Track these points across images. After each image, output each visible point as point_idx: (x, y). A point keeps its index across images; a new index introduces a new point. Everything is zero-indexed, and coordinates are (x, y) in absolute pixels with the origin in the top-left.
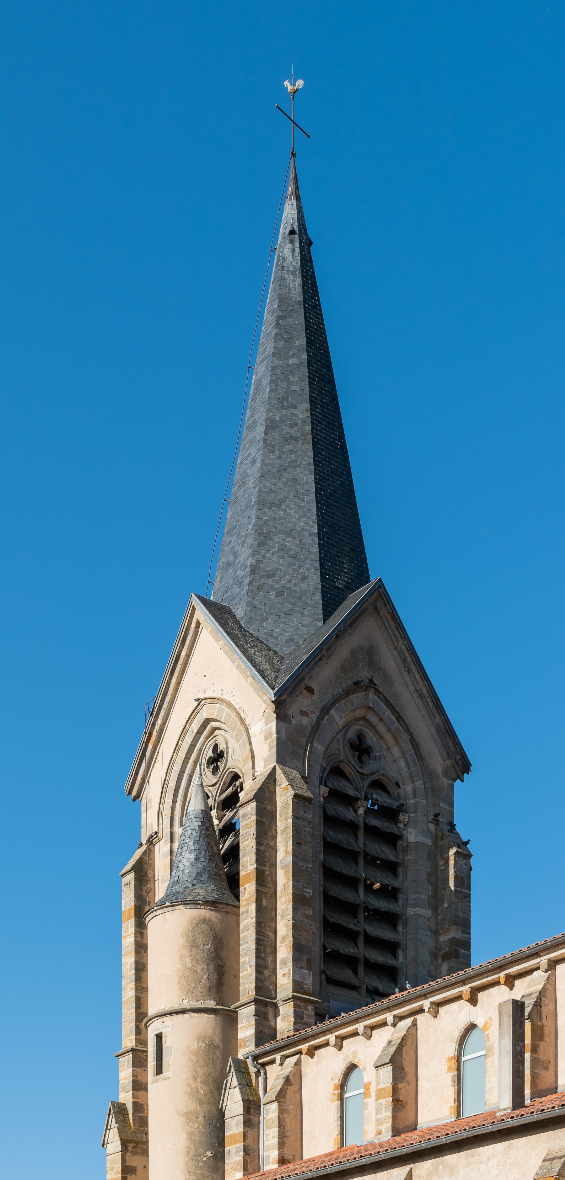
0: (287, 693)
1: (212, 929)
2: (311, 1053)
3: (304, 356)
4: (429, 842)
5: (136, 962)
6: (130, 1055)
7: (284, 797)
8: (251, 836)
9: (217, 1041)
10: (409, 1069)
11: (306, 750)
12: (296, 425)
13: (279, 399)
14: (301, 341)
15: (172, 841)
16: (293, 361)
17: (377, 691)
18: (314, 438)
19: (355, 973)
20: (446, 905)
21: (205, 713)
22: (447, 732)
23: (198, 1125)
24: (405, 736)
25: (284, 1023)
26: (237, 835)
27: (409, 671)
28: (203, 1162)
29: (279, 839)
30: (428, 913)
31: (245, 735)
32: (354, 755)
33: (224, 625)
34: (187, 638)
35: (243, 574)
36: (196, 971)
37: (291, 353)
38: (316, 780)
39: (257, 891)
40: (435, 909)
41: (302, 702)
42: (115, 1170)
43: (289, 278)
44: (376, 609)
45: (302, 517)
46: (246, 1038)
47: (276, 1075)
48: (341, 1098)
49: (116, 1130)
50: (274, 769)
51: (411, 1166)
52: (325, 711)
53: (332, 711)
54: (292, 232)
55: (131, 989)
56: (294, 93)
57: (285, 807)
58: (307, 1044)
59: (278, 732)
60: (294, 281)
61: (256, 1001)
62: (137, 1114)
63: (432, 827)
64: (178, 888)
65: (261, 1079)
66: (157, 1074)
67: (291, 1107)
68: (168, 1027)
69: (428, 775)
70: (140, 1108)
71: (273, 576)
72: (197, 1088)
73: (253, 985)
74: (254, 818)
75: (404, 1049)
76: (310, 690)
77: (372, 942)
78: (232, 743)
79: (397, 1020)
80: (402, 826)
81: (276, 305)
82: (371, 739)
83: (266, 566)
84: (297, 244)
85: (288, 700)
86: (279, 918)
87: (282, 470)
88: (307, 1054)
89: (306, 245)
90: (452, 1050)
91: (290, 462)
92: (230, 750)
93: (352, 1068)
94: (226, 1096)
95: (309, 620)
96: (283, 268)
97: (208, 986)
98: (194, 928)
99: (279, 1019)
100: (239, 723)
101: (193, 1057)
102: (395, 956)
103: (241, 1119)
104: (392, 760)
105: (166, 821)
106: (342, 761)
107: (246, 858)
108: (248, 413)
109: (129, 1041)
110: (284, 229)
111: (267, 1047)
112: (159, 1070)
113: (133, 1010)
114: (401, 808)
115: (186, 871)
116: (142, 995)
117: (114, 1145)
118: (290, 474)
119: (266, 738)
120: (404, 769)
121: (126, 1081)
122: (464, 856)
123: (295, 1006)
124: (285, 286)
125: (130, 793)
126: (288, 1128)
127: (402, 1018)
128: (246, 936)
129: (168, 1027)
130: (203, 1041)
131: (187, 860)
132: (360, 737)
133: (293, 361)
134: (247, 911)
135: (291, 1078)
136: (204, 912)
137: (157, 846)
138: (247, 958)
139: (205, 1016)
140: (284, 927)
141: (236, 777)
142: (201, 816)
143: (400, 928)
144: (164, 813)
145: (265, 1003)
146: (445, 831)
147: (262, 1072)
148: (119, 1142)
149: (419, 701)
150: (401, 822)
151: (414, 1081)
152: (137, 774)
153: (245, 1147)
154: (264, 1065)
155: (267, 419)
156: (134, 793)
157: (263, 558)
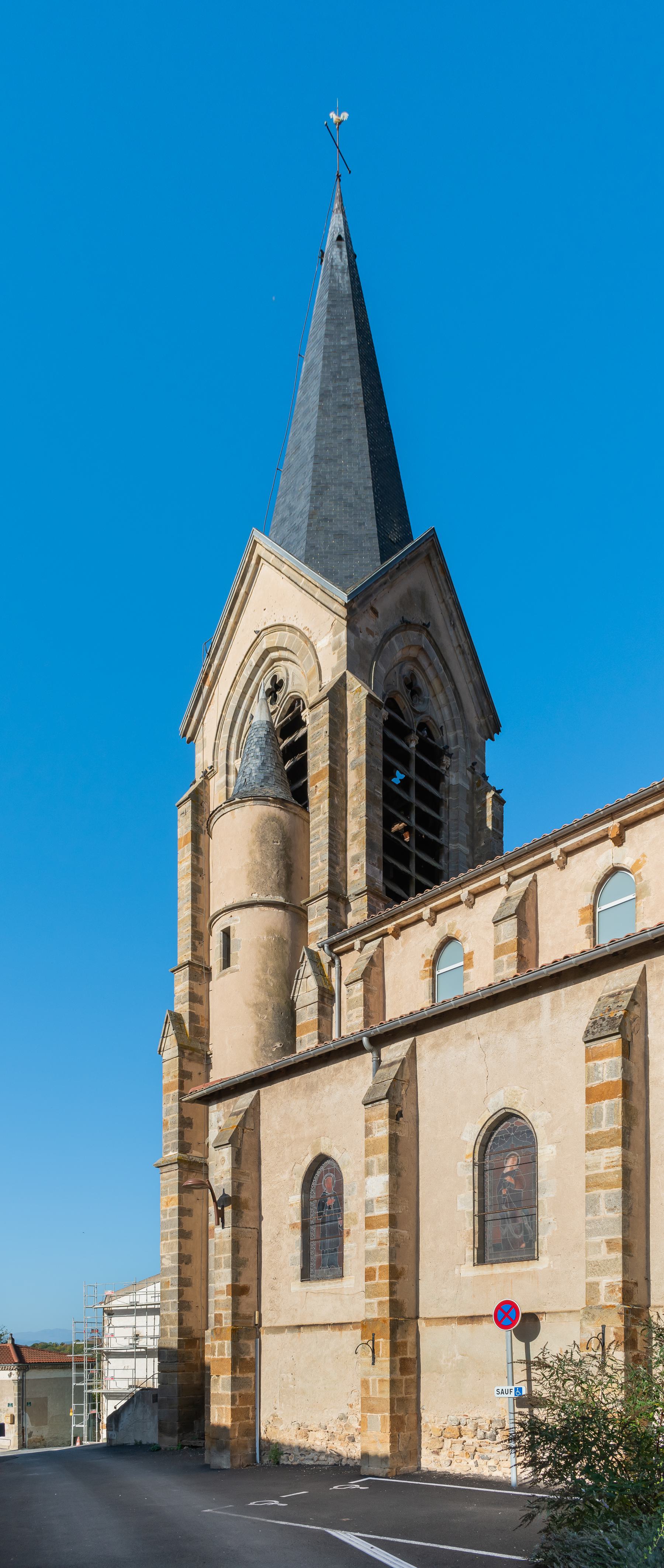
0: (359, 601)
1: (282, 827)
2: (396, 934)
5: (193, 883)
6: (187, 969)
7: (357, 695)
8: (324, 734)
9: (286, 936)
10: (531, 926)
11: (372, 667)
12: (349, 395)
13: (332, 373)
14: (352, 327)
15: (228, 772)
17: (429, 634)
18: (365, 408)
20: (483, 844)
22: (483, 691)
23: (268, 1017)
24: (449, 686)
25: (357, 913)
27: (454, 626)
28: (272, 1052)
29: (350, 741)
30: (466, 850)
31: (310, 653)
32: (407, 692)
36: (266, 866)
37: (342, 336)
39: (330, 787)
40: (472, 848)
42: (171, 1075)
43: (338, 275)
44: (428, 558)
46: (317, 931)
48: (433, 975)
49: (174, 1036)
50: (345, 674)
51: (644, 962)
52: (387, 636)
53: (393, 639)
54: (339, 238)
55: (188, 908)
56: (340, 123)
57: (358, 708)
58: (394, 923)
59: (348, 640)
60: (343, 278)
62: (193, 1024)
63: (470, 774)
65: (334, 971)
66: (224, 968)
67: (375, 988)
68: (236, 920)
69: (467, 727)
71: (331, 521)
72: (266, 980)
73: (327, 878)
74: (327, 716)
75: (527, 902)
76: (376, 613)
79: (511, 879)
80: (444, 768)
81: (326, 297)
82: (421, 683)
84: (344, 249)
85: (358, 610)
86: (349, 817)
87: (337, 431)
88: (392, 934)
90: (586, 899)
91: (345, 425)
92: (290, 677)
94: (298, 986)
96: (332, 266)
97: (277, 881)
98: (263, 824)
99: (350, 915)
100: (303, 643)
101: (262, 949)
103: (315, 1007)
104: (438, 708)
105: (222, 755)
106: (398, 693)
107: (317, 758)
108: (299, 393)
109: (184, 954)
110: (331, 237)
112: (226, 962)
113: (190, 928)
115: (254, 775)
116: (197, 915)
117: (171, 1050)
119: (334, 649)
120: (447, 718)
121: (182, 994)
122: (499, 801)
123: (369, 900)
124: (335, 281)
125: (184, 735)
126: (372, 1008)
127: (514, 877)
128: (318, 832)
129: (238, 922)
130: (273, 935)
132: (413, 675)
134: (319, 808)
135: (375, 959)
136: (273, 810)
137: (212, 781)
138: (318, 853)
139: (274, 911)
140: (356, 827)
142: (266, 726)
143: (443, 861)
144: (220, 743)
145: (337, 896)
146: (479, 781)
147: (337, 961)
148: (177, 1047)
149: (460, 657)
150: (444, 765)
151: (535, 939)
152: (192, 716)
153: (319, 1034)
154: (339, 954)
155: (321, 388)
156: (189, 735)
157: (321, 504)
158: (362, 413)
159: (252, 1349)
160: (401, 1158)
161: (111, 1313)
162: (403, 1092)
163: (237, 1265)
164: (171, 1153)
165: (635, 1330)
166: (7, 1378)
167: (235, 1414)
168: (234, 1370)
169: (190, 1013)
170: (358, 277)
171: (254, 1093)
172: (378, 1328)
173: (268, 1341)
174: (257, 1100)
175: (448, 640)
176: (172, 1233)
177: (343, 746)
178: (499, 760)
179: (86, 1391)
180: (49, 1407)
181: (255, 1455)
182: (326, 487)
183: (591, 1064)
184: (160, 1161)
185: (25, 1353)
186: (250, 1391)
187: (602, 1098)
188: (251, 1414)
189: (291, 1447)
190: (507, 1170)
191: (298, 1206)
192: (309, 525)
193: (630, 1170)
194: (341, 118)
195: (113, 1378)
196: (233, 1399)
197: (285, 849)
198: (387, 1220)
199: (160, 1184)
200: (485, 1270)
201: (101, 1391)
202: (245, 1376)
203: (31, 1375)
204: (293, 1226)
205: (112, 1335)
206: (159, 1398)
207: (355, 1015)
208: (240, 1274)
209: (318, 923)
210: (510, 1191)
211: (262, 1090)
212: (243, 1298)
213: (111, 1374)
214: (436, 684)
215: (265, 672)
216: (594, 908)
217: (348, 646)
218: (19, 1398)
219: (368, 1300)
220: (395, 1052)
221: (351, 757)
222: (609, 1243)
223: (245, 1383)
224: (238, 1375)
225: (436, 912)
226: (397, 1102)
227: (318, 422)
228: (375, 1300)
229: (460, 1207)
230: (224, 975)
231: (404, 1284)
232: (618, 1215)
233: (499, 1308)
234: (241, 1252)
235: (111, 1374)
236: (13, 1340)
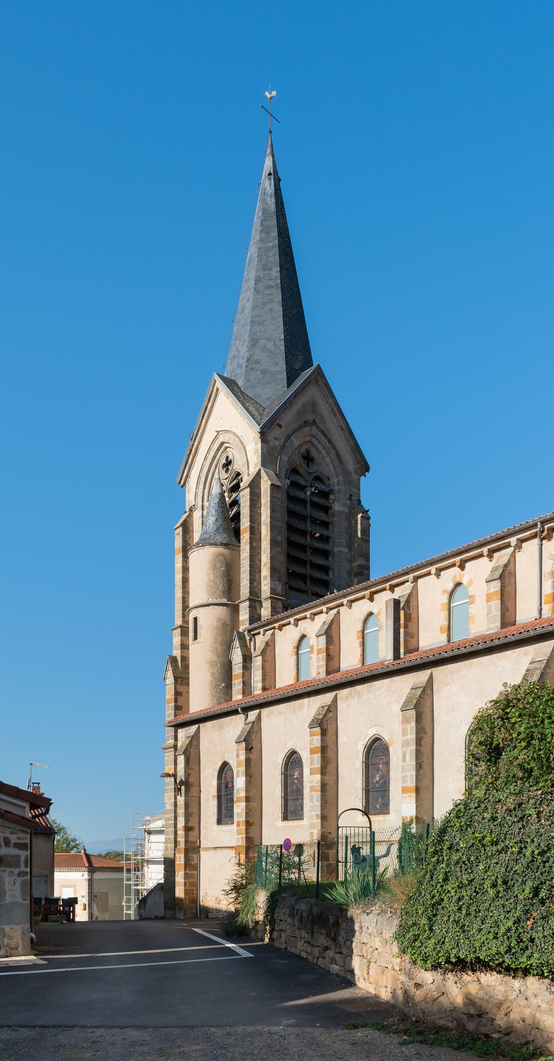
1: (225, 559)
2: (280, 628)
3: (277, 242)
4: (347, 510)
5: (183, 577)
9: (228, 622)
10: (335, 637)
12: (272, 279)
14: (275, 233)
15: (203, 509)
16: (270, 245)
17: (317, 426)
19: (305, 583)
21: (221, 439)
22: (356, 449)
23: (217, 668)
24: (333, 452)
25: (265, 612)
26: (239, 507)
27: (335, 415)
29: (262, 509)
30: (346, 550)
32: (304, 462)
33: (232, 390)
34: (212, 397)
35: (243, 362)
38: (283, 476)
39: (250, 538)
41: (275, 432)
43: (268, 199)
44: (316, 381)
45: (276, 330)
47: (260, 640)
50: (260, 470)
52: (288, 437)
53: (292, 438)
54: (270, 174)
56: (271, 98)
57: (266, 491)
59: (262, 449)
60: (271, 201)
61: (250, 599)
63: (348, 502)
64: (205, 536)
65: (252, 643)
67: (269, 659)
69: (346, 473)
70: (185, 659)
73: (248, 590)
76: (280, 426)
77: (315, 566)
78: (236, 455)
80: (331, 501)
81: (261, 214)
82: (314, 453)
83: (255, 357)
84: (272, 181)
86: (262, 553)
87: (264, 304)
89: (277, 181)
90: (359, 627)
93: (303, 637)
95: (279, 387)
96: (265, 194)
99: (262, 609)
101: (214, 630)
102: (327, 574)
103: (241, 665)
104: (326, 465)
105: (200, 499)
109: (178, 621)
111: (256, 625)
112: (195, 638)
114: (331, 492)
117: (170, 680)
118: (269, 307)
119: (255, 453)
120: (333, 470)
121: (177, 644)
122: (366, 518)
123: (272, 602)
124: (266, 203)
125: (180, 483)
126: (267, 670)
127: (331, 609)
129: (200, 613)
131: (211, 520)
132: (308, 452)
133: (270, 245)
134: (245, 549)
135: (269, 642)
136: (221, 550)
137: (194, 513)
139: (221, 608)
140: (265, 558)
141: (238, 474)
144: (199, 495)
145: (255, 601)
146: (355, 504)
147: (253, 639)
149: (341, 432)
153: (243, 681)
154: (254, 635)
155: (256, 276)
156: (182, 483)
157: (254, 353)
158: (280, 291)
159: (195, 859)
160: (252, 769)
161: (150, 833)
162: (254, 737)
163: (187, 816)
164: (170, 741)
165: (328, 853)
166: (81, 877)
167: (186, 891)
168: (185, 869)
169: (181, 656)
170: (281, 196)
171: (197, 726)
172: (241, 850)
173: (203, 854)
174: (198, 730)
175: (332, 426)
176: (171, 789)
177: (259, 511)
178: (370, 490)
179: (133, 887)
180: (109, 899)
181: (197, 913)
182: (257, 341)
183: (311, 738)
184: (164, 746)
185: (93, 860)
186: (195, 880)
187: (315, 753)
188: (195, 892)
189: (213, 909)
190: (295, 777)
191: (216, 787)
192: (247, 366)
193: (326, 784)
194: (272, 95)
195: (150, 879)
196: (185, 883)
197: (227, 571)
198: (244, 799)
199: (164, 759)
200: (286, 823)
201: (143, 888)
202: (192, 872)
203: (97, 876)
204: (214, 796)
205: (150, 848)
206: (164, 887)
207: (258, 675)
208: (189, 820)
209: (244, 615)
210: (296, 787)
211: (201, 725)
212: (191, 833)
213: (149, 876)
214: (324, 452)
215: (223, 453)
216: (363, 632)
217: (262, 453)
218: (89, 892)
219: (238, 836)
220: (253, 715)
221: (263, 518)
222: (317, 815)
223: (192, 876)
224: (188, 872)
225: (298, 620)
226: (250, 742)
227: (253, 299)
228: (240, 836)
229: (277, 793)
230: (195, 643)
231: (253, 830)
232: (319, 804)
233: (285, 841)
234: (190, 809)
235: (149, 876)
236: (85, 850)
